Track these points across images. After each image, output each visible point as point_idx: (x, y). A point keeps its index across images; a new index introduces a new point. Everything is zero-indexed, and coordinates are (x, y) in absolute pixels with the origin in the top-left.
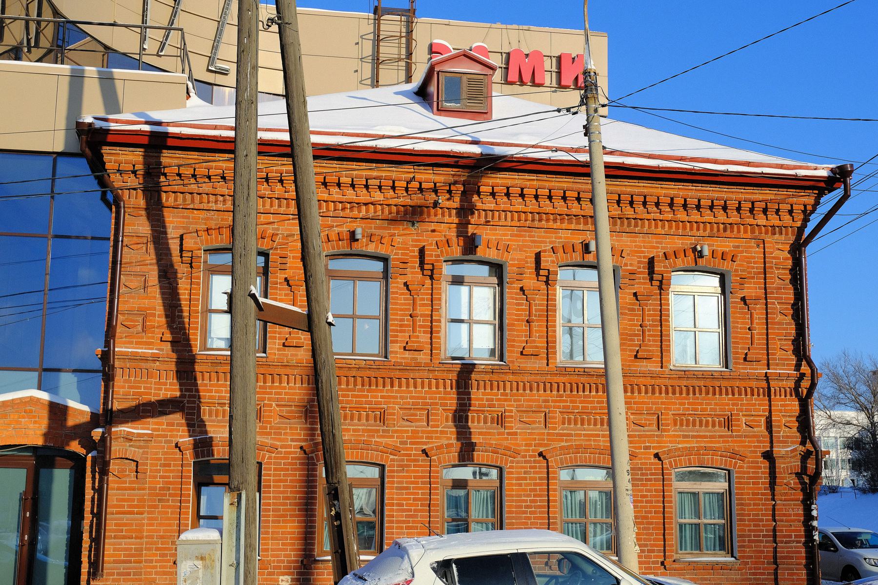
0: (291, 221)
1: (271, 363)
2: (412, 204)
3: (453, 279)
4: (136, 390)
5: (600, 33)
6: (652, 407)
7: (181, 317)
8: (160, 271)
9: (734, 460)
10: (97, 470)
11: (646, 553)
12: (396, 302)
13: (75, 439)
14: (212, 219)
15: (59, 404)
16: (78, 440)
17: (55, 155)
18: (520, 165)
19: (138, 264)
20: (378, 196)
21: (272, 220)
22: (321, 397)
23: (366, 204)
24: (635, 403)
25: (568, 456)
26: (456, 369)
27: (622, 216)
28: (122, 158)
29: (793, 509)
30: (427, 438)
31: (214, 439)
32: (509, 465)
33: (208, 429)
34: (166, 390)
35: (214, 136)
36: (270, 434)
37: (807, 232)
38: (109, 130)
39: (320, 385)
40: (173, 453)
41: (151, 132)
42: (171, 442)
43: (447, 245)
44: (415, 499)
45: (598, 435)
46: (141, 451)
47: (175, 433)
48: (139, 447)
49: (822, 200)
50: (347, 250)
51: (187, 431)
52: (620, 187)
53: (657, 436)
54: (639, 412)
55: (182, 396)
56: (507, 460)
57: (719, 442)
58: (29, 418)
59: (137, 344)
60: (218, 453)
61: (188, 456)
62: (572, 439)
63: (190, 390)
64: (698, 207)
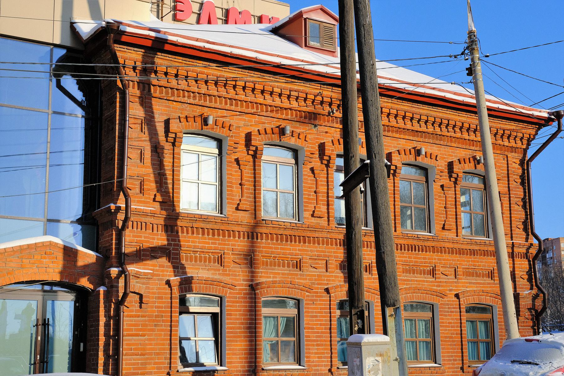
0: (238, 117)
1: (230, 222)
2: (315, 112)
3: (337, 168)
4: (138, 239)
5: (285, 4)
6: (467, 264)
7: (166, 183)
8: (152, 147)
9: (496, 300)
10: (114, 301)
12: (306, 182)
13: (84, 276)
14: (186, 110)
15: (72, 248)
16: (87, 277)
17: (52, 47)
18: (383, 92)
19: (137, 140)
20: (294, 104)
21: (225, 115)
22: (354, 245)
23: (286, 109)
25: (409, 295)
27: (434, 133)
28: (128, 55)
29: (528, 332)
30: (327, 280)
31: (194, 278)
32: (376, 300)
33: (187, 270)
34: (158, 239)
35: (200, 47)
36: (229, 275)
37: (530, 154)
38: (125, 32)
39: (353, 236)
40: (164, 289)
41: (156, 38)
42: (162, 280)
43: (338, 143)
44: (321, 325)
46: (144, 286)
47: (165, 273)
48: (143, 284)
49: (539, 132)
50: (277, 142)
51: (172, 271)
52: (437, 113)
53: (455, 282)
55: (169, 244)
56: (374, 297)
57: (487, 287)
58: (49, 259)
59: (138, 203)
60: (196, 289)
61: (176, 291)
62: (410, 283)
63: (175, 240)
64: (468, 130)
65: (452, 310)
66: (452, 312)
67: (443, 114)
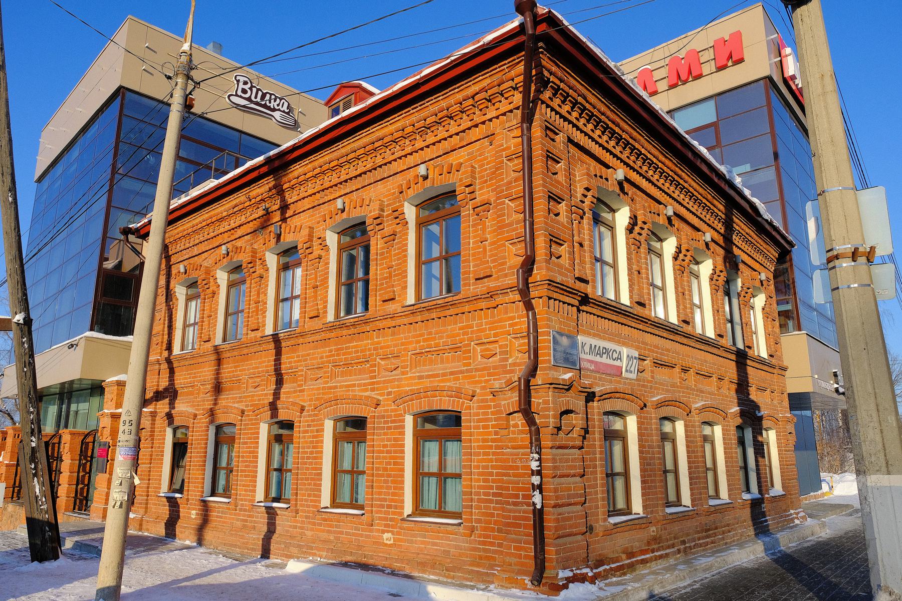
6: (394, 350)
9: (452, 399)
11: (385, 509)
24: (382, 348)
26: (596, 321)
45: (354, 385)
52: (361, 140)
54: (385, 357)
65: (390, 425)
66: (389, 428)
67: (370, 136)
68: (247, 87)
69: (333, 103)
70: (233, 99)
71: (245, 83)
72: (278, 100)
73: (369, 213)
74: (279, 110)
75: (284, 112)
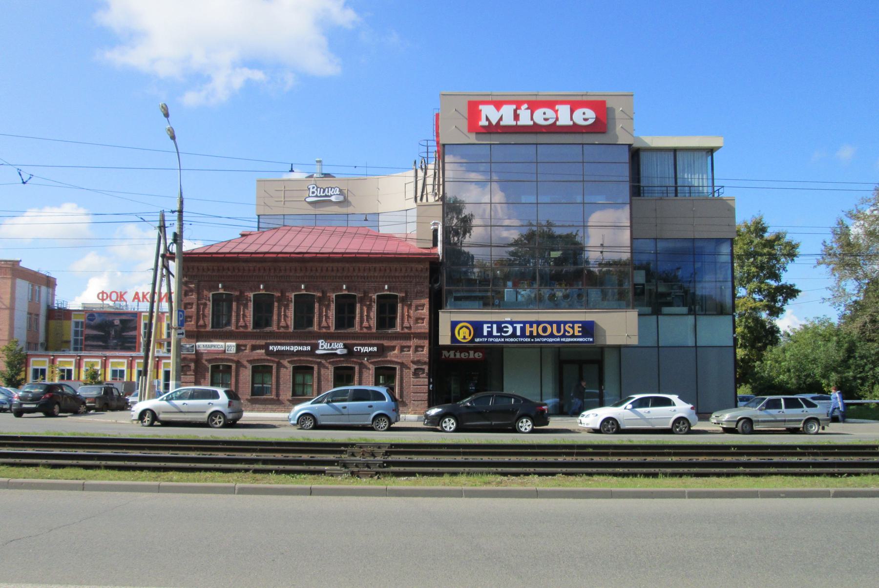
68: (314, 190)
69: (394, 175)
70: (307, 200)
71: (313, 188)
72: (333, 189)
73: (861, 205)
74: (334, 195)
75: (337, 195)
